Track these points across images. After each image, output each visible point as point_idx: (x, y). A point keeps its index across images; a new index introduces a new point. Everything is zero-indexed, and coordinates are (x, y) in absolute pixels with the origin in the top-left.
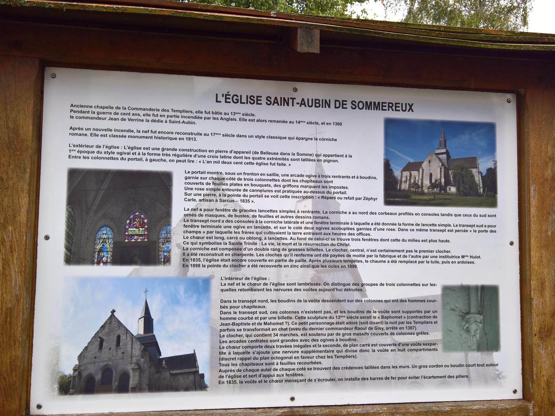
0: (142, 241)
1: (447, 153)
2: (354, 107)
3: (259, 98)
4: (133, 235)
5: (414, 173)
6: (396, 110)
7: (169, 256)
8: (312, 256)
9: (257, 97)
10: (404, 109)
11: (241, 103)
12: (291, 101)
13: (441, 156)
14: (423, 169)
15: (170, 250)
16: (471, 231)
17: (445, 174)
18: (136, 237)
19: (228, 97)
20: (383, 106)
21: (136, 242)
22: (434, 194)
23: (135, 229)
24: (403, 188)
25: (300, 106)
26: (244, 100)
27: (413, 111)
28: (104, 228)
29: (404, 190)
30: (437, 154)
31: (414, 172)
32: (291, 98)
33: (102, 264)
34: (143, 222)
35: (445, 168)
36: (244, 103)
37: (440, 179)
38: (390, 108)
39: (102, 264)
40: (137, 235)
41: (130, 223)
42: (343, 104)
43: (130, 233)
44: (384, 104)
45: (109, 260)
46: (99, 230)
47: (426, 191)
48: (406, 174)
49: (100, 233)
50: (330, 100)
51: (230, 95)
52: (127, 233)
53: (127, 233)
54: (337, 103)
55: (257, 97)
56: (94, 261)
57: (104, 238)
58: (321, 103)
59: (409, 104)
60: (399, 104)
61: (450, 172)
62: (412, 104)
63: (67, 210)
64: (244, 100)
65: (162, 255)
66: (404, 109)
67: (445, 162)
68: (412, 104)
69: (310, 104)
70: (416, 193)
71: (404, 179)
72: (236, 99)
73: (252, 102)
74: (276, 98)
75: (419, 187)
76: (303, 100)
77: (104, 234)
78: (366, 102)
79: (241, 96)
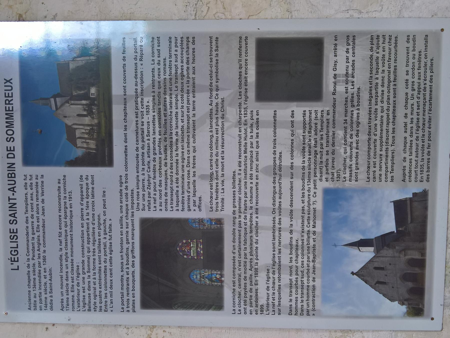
0: (203, 243)
1: (55, 97)
2: (12, 140)
3: (12, 231)
4: (198, 253)
5: (78, 134)
6: (12, 97)
7: (215, 220)
8: (183, 166)
9: (10, 233)
10: (10, 88)
11: (17, 247)
12: (12, 201)
13: (59, 104)
14: (74, 124)
15: (210, 219)
16: (142, 65)
17: (78, 100)
18: (199, 250)
19: (13, 260)
20: (9, 110)
21: (203, 249)
22: (99, 112)
23: (192, 251)
24: (94, 147)
25: (15, 192)
26: (14, 245)
27: (11, 79)
28: (191, 277)
29: (96, 145)
30: (57, 109)
31: (77, 134)
32: (9, 201)
33: (223, 279)
34: (185, 243)
35: (71, 99)
36: (17, 245)
37: (83, 105)
38: (10, 103)
39: (223, 279)
40: (197, 249)
41: (187, 255)
42: (10, 150)
43: (195, 255)
44: (7, 109)
45: (219, 273)
46: (193, 281)
47: (96, 121)
48: (79, 142)
49: (196, 280)
50: (8, 164)
51: (11, 258)
52: (196, 258)
53: (196, 258)
54: (10, 156)
55: (10, 233)
56: (219, 286)
57: (200, 277)
58: (11, 172)
59: (5, 83)
60: (5, 93)
61: (75, 93)
62: (5, 79)
63: (176, 309)
64: (14, 245)
65: (214, 226)
66: (10, 88)
67: (64, 99)
68: (5, 79)
69: (13, 182)
70: (99, 133)
71: (85, 145)
72: (15, 252)
73: (15, 237)
74: (10, 215)
75: (92, 129)
76: (9, 189)
77: (196, 277)
78: (7, 127)
79: (11, 248)
